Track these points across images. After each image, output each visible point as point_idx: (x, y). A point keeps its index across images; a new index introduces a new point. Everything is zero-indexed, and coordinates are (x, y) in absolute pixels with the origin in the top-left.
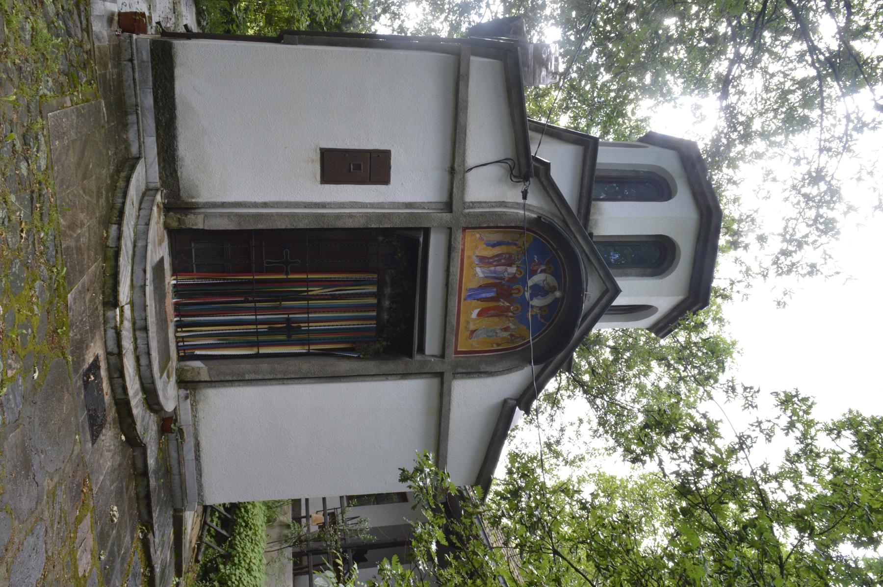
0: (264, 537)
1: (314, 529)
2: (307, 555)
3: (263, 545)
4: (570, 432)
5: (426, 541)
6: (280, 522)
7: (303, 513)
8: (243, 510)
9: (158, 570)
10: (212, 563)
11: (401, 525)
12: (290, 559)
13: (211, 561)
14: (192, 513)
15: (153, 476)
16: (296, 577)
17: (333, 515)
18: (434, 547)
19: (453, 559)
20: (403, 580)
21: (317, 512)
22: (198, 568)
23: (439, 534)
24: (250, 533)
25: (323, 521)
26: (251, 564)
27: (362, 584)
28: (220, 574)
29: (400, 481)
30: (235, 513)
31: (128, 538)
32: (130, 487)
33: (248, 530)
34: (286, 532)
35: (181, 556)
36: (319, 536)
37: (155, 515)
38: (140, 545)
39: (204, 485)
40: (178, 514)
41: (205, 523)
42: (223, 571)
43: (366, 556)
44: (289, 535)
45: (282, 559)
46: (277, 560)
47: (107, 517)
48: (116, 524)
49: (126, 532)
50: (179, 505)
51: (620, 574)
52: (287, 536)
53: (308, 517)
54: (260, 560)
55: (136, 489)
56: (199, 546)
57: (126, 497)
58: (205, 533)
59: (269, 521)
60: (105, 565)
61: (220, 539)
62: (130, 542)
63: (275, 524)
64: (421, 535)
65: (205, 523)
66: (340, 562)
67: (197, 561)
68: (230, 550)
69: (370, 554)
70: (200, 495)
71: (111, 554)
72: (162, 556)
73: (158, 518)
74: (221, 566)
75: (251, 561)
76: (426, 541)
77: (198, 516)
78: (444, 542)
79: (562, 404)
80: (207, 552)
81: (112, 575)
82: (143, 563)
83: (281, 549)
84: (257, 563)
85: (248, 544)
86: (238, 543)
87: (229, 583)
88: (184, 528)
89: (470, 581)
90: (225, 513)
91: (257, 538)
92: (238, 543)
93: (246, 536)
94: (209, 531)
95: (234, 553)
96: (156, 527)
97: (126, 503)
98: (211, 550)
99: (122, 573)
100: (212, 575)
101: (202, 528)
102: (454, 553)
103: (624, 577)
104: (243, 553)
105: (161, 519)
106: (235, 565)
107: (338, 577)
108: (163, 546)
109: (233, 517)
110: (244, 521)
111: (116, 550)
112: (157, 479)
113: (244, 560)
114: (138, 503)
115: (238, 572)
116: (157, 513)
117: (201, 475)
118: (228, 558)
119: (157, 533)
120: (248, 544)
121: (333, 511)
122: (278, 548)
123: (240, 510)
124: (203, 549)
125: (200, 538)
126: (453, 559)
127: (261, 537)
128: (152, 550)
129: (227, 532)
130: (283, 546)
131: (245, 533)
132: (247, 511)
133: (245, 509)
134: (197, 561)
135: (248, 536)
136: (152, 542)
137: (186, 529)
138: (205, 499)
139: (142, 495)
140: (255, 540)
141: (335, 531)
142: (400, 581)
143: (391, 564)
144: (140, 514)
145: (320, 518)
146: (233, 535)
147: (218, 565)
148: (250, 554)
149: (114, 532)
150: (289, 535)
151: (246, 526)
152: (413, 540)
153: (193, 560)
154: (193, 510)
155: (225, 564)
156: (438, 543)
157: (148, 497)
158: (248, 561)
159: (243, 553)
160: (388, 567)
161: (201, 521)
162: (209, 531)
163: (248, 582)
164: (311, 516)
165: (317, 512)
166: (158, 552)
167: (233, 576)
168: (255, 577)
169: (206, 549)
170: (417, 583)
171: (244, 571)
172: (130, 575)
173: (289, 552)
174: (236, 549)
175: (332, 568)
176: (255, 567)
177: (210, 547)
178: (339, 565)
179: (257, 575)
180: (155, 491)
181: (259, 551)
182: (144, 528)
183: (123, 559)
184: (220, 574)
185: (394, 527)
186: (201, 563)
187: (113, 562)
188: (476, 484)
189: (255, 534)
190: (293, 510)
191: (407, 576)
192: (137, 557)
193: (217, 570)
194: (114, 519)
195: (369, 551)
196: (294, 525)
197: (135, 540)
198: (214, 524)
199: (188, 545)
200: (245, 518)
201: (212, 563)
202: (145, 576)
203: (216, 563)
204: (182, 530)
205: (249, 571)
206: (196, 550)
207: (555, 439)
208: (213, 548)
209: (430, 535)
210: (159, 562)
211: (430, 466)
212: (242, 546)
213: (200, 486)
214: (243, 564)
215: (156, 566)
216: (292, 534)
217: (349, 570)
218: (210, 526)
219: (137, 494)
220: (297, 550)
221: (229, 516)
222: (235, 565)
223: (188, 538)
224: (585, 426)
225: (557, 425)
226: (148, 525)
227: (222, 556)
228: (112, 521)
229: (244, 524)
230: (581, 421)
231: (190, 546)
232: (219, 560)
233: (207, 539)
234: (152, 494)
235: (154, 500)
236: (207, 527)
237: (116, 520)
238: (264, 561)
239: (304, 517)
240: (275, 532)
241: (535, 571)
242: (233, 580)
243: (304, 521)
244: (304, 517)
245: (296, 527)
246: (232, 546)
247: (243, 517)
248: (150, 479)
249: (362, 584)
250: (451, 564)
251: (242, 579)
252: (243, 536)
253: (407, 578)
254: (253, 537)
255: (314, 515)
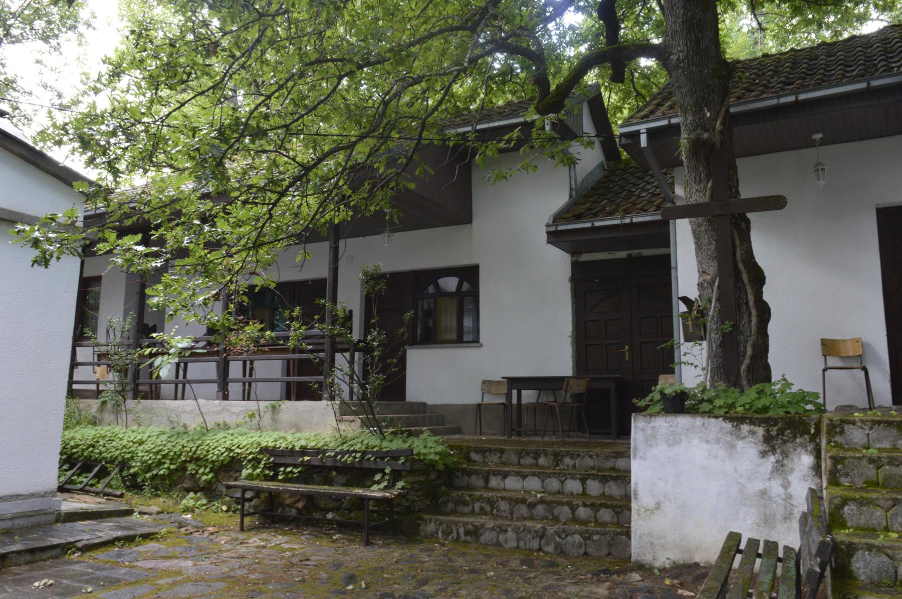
0: (109, 428)
1: (111, 376)
2: (138, 385)
3: (117, 429)
4: (49, 78)
5: (134, 256)
6: (98, 411)
7: (93, 387)
8: (75, 450)
9: (119, 533)
10: (127, 481)
11: (127, 285)
12: (139, 403)
13: (124, 482)
14: (64, 503)
15: (7, 548)
16: (161, 396)
17: (100, 356)
18: (141, 248)
19: (157, 231)
20: (171, 286)
21: (94, 373)
22: (129, 495)
23: (129, 241)
24: (102, 443)
25: (106, 366)
26: (135, 441)
27: (174, 330)
28: (139, 471)
29: (46, 267)
30: (76, 459)
31: (77, 567)
32: (16, 571)
33: (98, 444)
34: (109, 405)
35: (111, 511)
36: (118, 371)
37: (56, 541)
38: (88, 554)
39: (32, 491)
40: (62, 518)
41: (82, 490)
42: (136, 469)
43: (150, 326)
44: (113, 402)
45: (137, 410)
46: (137, 415)
47: (44, 592)
48: (56, 581)
49: (69, 570)
50: (52, 518)
51: (195, 63)
52: (114, 405)
53: (97, 383)
54: (133, 432)
55: (20, 565)
56: (106, 494)
57: (27, 575)
58: (93, 489)
59: (94, 424)
60: (99, 586)
61: (103, 473)
62: (79, 564)
63: (99, 417)
64: (127, 260)
65: (82, 490)
66: (149, 350)
67: (122, 496)
68: (116, 462)
69: (149, 321)
70: (44, 495)
71: (87, 582)
72: (106, 530)
73: (60, 538)
74: (132, 471)
75: (132, 441)
76: (134, 256)
77: (72, 498)
78: (139, 237)
79: (10, 76)
80: (114, 487)
81: (112, 578)
82: (109, 548)
83: (126, 411)
84: (135, 434)
85: (114, 444)
86: (110, 454)
87: (150, 462)
88: (81, 511)
89: (183, 219)
90: (75, 469)
91: (109, 435)
92: (110, 454)
93: (104, 446)
94: (92, 485)
95: (120, 459)
96: (71, 540)
97: (34, 573)
98: (113, 483)
99: (113, 568)
100: (139, 480)
101: (87, 492)
102: (151, 229)
103: (199, 59)
104: (122, 449)
105: (63, 535)
106: (132, 457)
107: (163, 354)
108: (94, 531)
109: (81, 461)
110: (88, 448)
111: (85, 577)
112: (13, 543)
113: (130, 447)
114: (38, 561)
115: (140, 454)
116: (55, 539)
117: (18, 496)
118: (124, 465)
119: (78, 538)
120: (114, 444)
121: (96, 356)
122: (124, 414)
123: (74, 453)
124: (110, 490)
125: (97, 494)
126: (157, 231)
127: (108, 431)
128: (96, 541)
129: (96, 466)
130: (124, 409)
131: (100, 448)
132: (77, 446)
133: (74, 448)
134: (122, 496)
135: (104, 444)
136: (86, 542)
137: (81, 509)
138: (49, 490)
139: (29, 558)
140: (111, 437)
141: (116, 354)
142: (172, 289)
143: (153, 296)
144: (52, 558)
145: (101, 370)
146: (101, 460)
147: (130, 475)
148: (125, 442)
149: (65, 582)
150: (113, 402)
151: (93, 446)
152: (131, 270)
153: (119, 499)
154: (60, 502)
155: (130, 467)
156: (137, 244)
157: (32, 551)
158: (131, 444)
159: (122, 449)
160: (155, 300)
161: (78, 494)
162: (92, 485)
163: (152, 444)
164: (98, 379)
165: (94, 373)
166: (100, 534)
167: (144, 458)
168: (149, 437)
169: (111, 487)
170: (175, 272)
171: (141, 448)
172: (118, 560)
173: (130, 403)
174: (117, 457)
175: (153, 359)
176: (139, 437)
177: (109, 483)
178: (151, 353)
179: (147, 434)
180: (28, 544)
181: (124, 433)
182: (69, 552)
183: (99, 569)
184: (139, 471)
185: (126, 294)
186: (124, 491)
187: (98, 579)
188: (72, 186)
189: (104, 437)
190: (88, 398)
191: (167, 281)
192: (100, 555)
193: (135, 475)
194: (49, 583)
195: (145, 322)
196: (103, 397)
197: (81, 559)
198: (85, 480)
199: (101, 506)
200: (84, 447)
201: (127, 481)
202: (123, 545)
203: (127, 476)
204: (82, 513)
205: (141, 443)
206: (110, 497)
207: (56, 98)
208: (112, 479)
209: (129, 250)
210: (111, 532)
211: (33, 231)
212: (114, 450)
213: (32, 495)
214: (132, 449)
215: (114, 536)
216: (112, 399)
217: (162, 344)
218: (86, 485)
219: (27, 563)
220: (130, 394)
221: (79, 464)
222: (132, 457)
223: (93, 506)
224: (45, 58)
225: (38, 91)
226: (67, 548)
227: (121, 471)
228: (51, 585)
229: (91, 449)
230: (38, 62)
231: (103, 503)
232: (125, 473)
233: (100, 487)
234: (30, 547)
235: (42, 544)
236: (88, 488)
237: (51, 581)
238: (135, 428)
239: (98, 387)
240: (108, 417)
241: (178, 149)
242: (148, 458)
243: (101, 387)
244: (98, 387)
245: (106, 395)
246: (112, 461)
247: (83, 450)
248: (10, 550)
249: (174, 330)
250: (162, 235)
251: (148, 449)
252: (104, 449)
253: (169, 281)
254: (107, 439)
255: (98, 376)
